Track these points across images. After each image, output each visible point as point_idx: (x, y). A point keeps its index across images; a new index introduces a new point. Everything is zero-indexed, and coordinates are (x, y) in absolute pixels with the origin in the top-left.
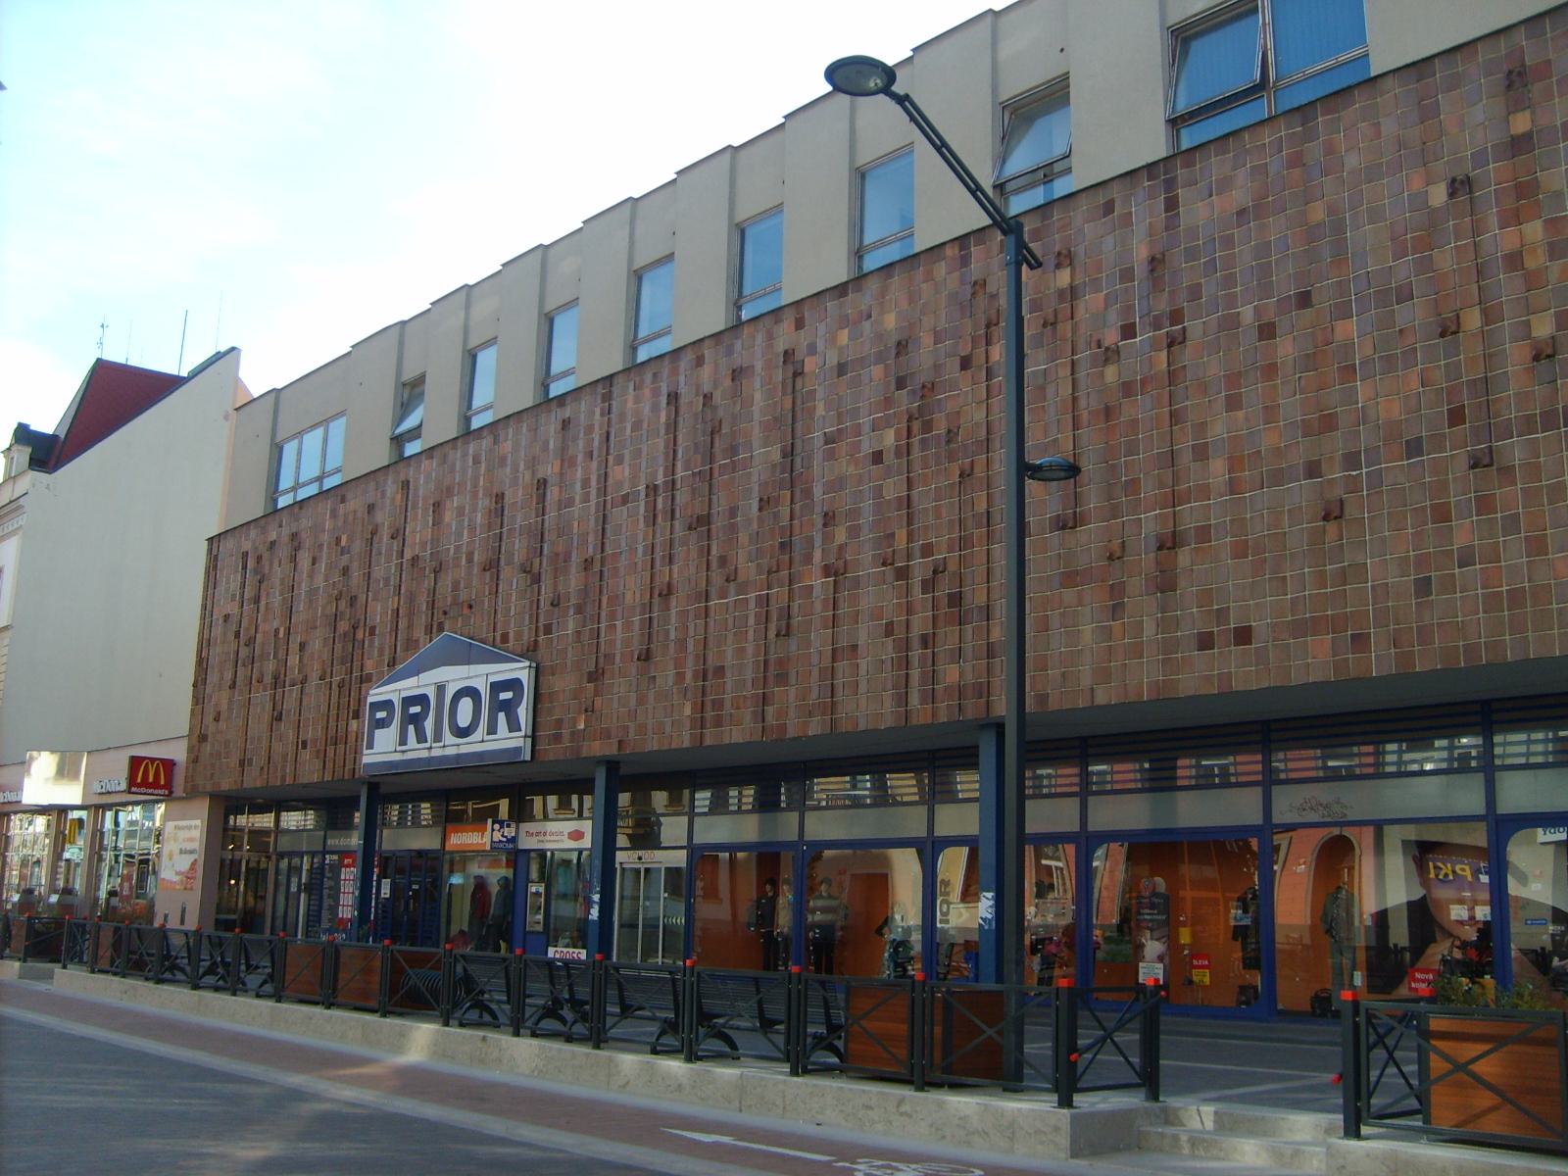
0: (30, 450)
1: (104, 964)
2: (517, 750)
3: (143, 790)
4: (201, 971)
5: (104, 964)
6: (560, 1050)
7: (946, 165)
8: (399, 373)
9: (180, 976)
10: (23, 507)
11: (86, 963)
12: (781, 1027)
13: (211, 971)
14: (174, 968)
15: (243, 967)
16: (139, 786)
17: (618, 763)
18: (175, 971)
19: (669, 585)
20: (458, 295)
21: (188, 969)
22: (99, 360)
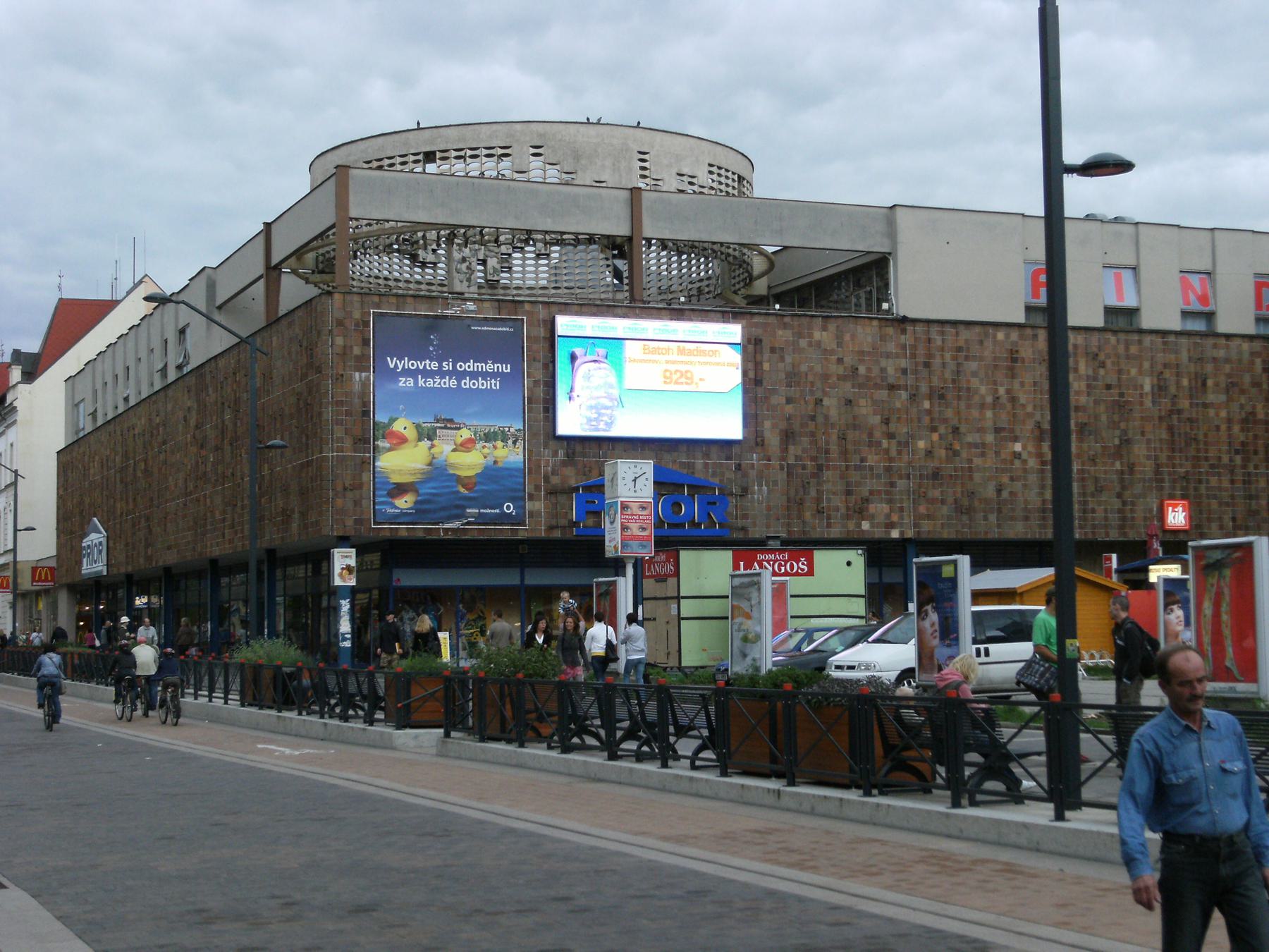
0: (21, 367)
1: (493, 729)
2: (102, 571)
3: (40, 584)
4: (619, 734)
5: (493, 729)
6: (416, 737)
7: (251, 280)
8: (177, 326)
9: (591, 741)
10: (16, 407)
11: (472, 728)
12: (556, 718)
13: (630, 735)
14: (583, 730)
15: (672, 729)
16: (37, 582)
17: (132, 575)
18: (584, 736)
19: (205, 473)
20: (257, 238)
21: (602, 733)
22: (61, 299)
